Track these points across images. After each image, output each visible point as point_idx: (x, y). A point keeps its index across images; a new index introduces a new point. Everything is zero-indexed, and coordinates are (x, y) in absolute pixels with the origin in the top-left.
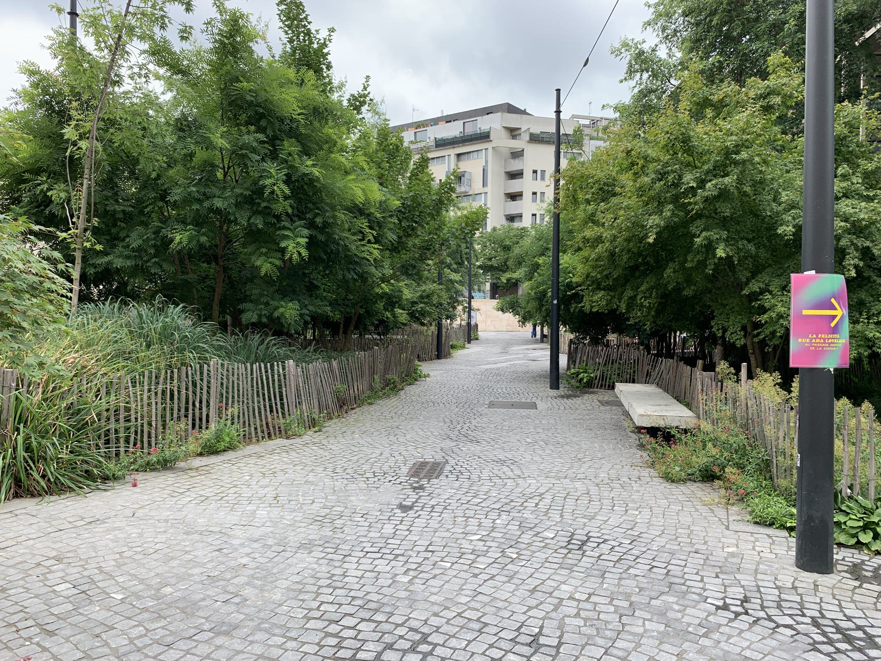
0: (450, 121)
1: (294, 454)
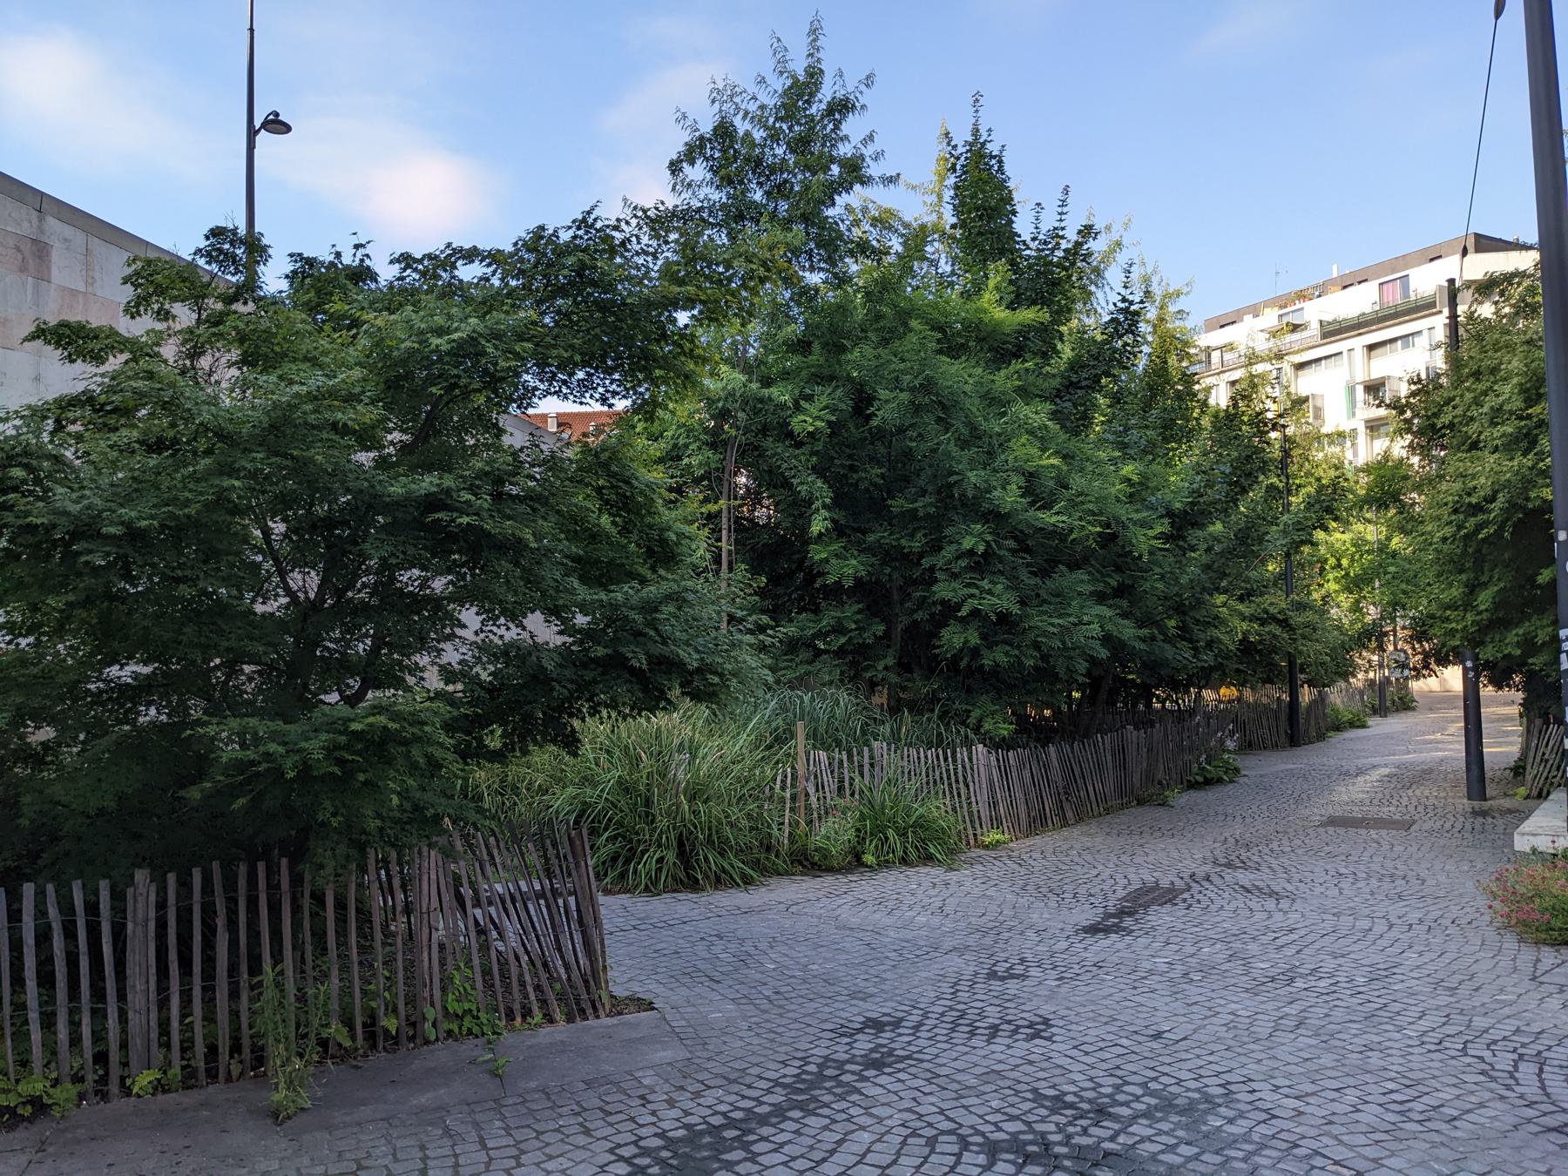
0: (1366, 280)
1: (980, 867)
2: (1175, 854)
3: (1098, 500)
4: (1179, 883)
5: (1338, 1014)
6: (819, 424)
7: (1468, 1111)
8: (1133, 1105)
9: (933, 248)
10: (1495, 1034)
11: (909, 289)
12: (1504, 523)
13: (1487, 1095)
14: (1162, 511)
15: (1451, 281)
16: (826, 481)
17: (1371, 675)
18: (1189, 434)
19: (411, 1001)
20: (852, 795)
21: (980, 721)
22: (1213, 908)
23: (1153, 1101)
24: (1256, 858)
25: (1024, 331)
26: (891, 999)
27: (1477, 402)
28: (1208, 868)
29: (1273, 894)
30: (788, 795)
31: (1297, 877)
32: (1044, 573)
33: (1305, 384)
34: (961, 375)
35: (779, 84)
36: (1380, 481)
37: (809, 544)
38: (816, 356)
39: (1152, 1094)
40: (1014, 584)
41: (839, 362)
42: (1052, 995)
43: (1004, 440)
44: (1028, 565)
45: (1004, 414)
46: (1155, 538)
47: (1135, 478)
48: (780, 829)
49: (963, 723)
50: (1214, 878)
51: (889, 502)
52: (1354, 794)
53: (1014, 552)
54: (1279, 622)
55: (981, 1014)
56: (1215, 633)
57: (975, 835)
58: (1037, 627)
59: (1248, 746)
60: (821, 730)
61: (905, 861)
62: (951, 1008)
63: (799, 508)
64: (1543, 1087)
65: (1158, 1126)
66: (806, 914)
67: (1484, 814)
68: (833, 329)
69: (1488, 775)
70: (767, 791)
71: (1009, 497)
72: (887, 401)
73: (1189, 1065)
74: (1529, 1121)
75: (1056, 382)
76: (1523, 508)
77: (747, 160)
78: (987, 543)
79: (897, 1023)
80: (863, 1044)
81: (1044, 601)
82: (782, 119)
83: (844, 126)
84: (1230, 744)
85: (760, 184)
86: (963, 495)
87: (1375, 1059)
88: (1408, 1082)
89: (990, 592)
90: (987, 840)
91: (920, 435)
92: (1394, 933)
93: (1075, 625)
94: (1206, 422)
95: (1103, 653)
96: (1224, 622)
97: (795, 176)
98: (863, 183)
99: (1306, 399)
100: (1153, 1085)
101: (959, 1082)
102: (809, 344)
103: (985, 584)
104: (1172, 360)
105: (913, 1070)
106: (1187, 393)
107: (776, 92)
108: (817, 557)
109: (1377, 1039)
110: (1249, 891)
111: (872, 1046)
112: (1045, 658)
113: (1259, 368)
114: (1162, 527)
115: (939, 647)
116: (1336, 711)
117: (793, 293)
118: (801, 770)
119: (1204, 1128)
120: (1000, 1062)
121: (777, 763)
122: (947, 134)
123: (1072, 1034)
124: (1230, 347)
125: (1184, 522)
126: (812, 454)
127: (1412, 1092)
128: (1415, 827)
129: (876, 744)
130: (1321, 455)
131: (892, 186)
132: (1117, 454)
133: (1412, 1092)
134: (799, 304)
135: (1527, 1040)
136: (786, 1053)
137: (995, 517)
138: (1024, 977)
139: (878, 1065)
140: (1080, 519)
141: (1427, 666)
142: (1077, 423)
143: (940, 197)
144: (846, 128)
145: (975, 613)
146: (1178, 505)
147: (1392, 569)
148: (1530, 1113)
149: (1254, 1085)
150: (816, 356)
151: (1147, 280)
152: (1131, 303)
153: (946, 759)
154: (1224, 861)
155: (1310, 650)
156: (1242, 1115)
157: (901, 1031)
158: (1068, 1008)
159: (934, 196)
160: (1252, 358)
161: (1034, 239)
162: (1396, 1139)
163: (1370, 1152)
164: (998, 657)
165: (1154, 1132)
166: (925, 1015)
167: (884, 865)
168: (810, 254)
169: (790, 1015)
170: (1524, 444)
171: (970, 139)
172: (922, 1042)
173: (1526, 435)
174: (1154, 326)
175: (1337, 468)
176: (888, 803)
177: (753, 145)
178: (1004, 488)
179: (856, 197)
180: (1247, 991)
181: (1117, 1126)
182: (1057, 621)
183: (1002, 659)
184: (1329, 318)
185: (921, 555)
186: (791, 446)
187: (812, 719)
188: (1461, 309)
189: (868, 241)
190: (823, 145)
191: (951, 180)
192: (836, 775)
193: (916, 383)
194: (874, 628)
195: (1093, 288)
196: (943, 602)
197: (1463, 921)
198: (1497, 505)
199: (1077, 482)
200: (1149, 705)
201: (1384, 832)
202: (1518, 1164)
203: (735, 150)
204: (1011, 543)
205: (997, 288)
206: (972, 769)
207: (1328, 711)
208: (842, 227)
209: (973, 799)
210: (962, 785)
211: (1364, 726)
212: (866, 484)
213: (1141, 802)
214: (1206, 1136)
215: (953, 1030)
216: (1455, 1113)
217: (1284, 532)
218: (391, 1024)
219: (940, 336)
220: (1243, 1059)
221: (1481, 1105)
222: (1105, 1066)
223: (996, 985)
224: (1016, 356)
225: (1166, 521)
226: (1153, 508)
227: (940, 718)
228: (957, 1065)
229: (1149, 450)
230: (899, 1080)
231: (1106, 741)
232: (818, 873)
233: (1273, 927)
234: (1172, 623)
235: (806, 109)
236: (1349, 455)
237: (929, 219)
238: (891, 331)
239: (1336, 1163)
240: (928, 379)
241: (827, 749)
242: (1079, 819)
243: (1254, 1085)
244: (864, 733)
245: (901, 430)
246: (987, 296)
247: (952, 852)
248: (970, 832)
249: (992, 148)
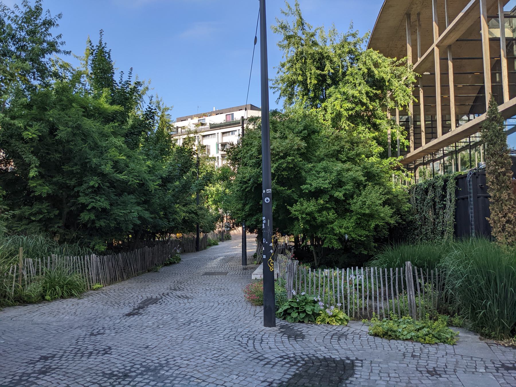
1: (91, 297)
2: (158, 287)
3: (138, 172)
4: (159, 297)
5: (202, 333)
6: (34, 136)
7: (234, 357)
8: (137, 371)
9: (84, 79)
10: (243, 333)
11: (74, 92)
12: (252, 187)
13: (240, 351)
14: (159, 177)
15: (243, 117)
16: (37, 157)
17: (220, 229)
18: (168, 153)
20: (42, 274)
21: (94, 246)
22: (169, 303)
23: (143, 369)
24: (183, 287)
25: (116, 112)
26: (52, 348)
27: (247, 153)
28: (168, 291)
29: (187, 298)
30: (14, 275)
31: (194, 291)
32: (120, 195)
33: (205, 142)
34: (89, 124)
35: (24, 10)
36: (223, 173)
37: (28, 180)
38: (34, 111)
39: (143, 367)
40: (108, 198)
41: (44, 114)
42: (113, 339)
43: (107, 149)
44: (114, 192)
45: (107, 140)
46: (157, 185)
47: (151, 166)
48: (10, 289)
49: (88, 247)
50: (170, 294)
51: (62, 167)
52: (213, 265)
53: (108, 187)
54: (194, 213)
55: (87, 349)
56: (175, 216)
57: (90, 286)
58: (116, 213)
59: (184, 252)
60: (30, 250)
61: (62, 297)
62: (75, 348)
63: (25, 167)
64: (254, 347)
65: (144, 377)
66: (19, 320)
67: (245, 269)
68: (42, 102)
69: (248, 258)
70: (5, 274)
71: (108, 168)
72: (62, 131)
73: (156, 355)
74: (250, 357)
75: (126, 131)
76: (257, 183)
77: (9, 35)
78: (99, 184)
79: (54, 356)
80: (39, 366)
81: (119, 205)
82: (24, 22)
83: (49, 30)
84: (178, 251)
85: (14, 45)
86: (91, 166)
87: (211, 345)
88: (219, 350)
89: (99, 201)
90: (95, 287)
91: (75, 144)
92: (219, 306)
93: (129, 213)
94: (174, 150)
95: (139, 222)
96: (178, 213)
97: (29, 44)
98: (56, 52)
99: (205, 146)
100: (144, 364)
101: (75, 374)
102: (32, 106)
103: (98, 198)
104: (165, 129)
105: (58, 372)
106: (169, 141)
107: (22, 12)
108: (32, 185)
109: (212, 339)
110: (180, 297)
111: (42, 366)
112: (118, 224)
113: (192, 135)
114: (159, 182)
115: (80, 220)
116: (210, 240)
117: (26, 87)
118: (20, 267)
119: (159, 375)
120: (92, 364)
121: (10, 263)
122: (90, 42)
123: (118, 351)
124: (183, 128)
125: (166, 181)
126: (31, 147)
127: (220, 353)
128: (228, 274)
129: (53, 255)
130: (208, 163)
131: (68, 55)
132: (146, 157)
133: (220, 353)
134: (28, 91)
135: (251, 334)
136: (6, 374)
137: (103, 175)
138: (103, 334)
139: (44, 373)
140: (132, 178)
141: (233, 227)
142: (134, 146)
143: (87, 62)
144: (50, 31)
145: (93, 208)
146: (164, 175)
147: (225, 198)
148: (250, 354)
149: (175, 359)
150: (34, 111)
151: (158, 103)
152: (152, 109)
153: (81, 260)
154: (173, 288)
155: (203, 223)
156: (171, 369)
157: (55, 359)
158: (118, 342)
159: (85, 62)
160: (189, 132)
161: (120, 83)
162: (215, 368)
163: (207, 374)
164: (102, 223)
165: (142, 379)
166: (65, 352)
167: (54, 299)
168: (34, 73)
169: (10, 359)
170: (257, 166)
171: (99, 45)
172: (63, 362)
173: (258, 163)
174: (160, 118)
175: (212, 168)
176: (57, 277)
177: (11, 29)
178: (106, 165)
179: (54, 56)
180: (176, 329)
181: (130, 380)
182: (123, 211)
183: (103, 224)
184: (212, 123)
185: (74, 187)
186: (23, 143)
187: (27, 246)
188: (245, 126)
189: (57, 73)
190: (41, 35)
191: (91, 57)
192: (36, 267)
193: (74, 125)
194: (54, 212)
195: (139, 102)
196: (83, 204)
197: (238, 301)
198: (251, 182)
199: (132, 165)
200: (154, 239)
201: (219, 276)
202: (246, 370)
203: (4, 30)
204: (108, 184)
205: (106, 97)
206: (90, 262)
207: (208, 240)
208: (47, 66)
209: (90, 273)
210: (86, 269)
211: (217, 245)
212: (53, 159)
213: (149, 271)
214: (159, 377)
215: (75, 356)
216: (231, 358)
217: (196, 186)
219: (84, 110)
220: (173, 351)
221: (238, 354)
222: (129, 360)
223: (93, 338)
224: (112, 121)
225: (160, 180)
226: (156, 176)
227: (79, 245)
228: (75, 368)
229: (155, 157)
230: (52, 377)
231: (138, 252)
232: (25, 304)
233: (186, 308)
234: (162, 213)
235: (34, 21)
236: (216, 164)
237: (83, 69)
238: (66, 106)
239: (197, 379)
240: (78, 124)
241: (32, 257)
242: (128, 278)
243: (175, 359)
244: (48, 251)
245: (68, 142)
246: (102, 99)
247: (81, 293)
248: (88, 285)
249: (107, 49)
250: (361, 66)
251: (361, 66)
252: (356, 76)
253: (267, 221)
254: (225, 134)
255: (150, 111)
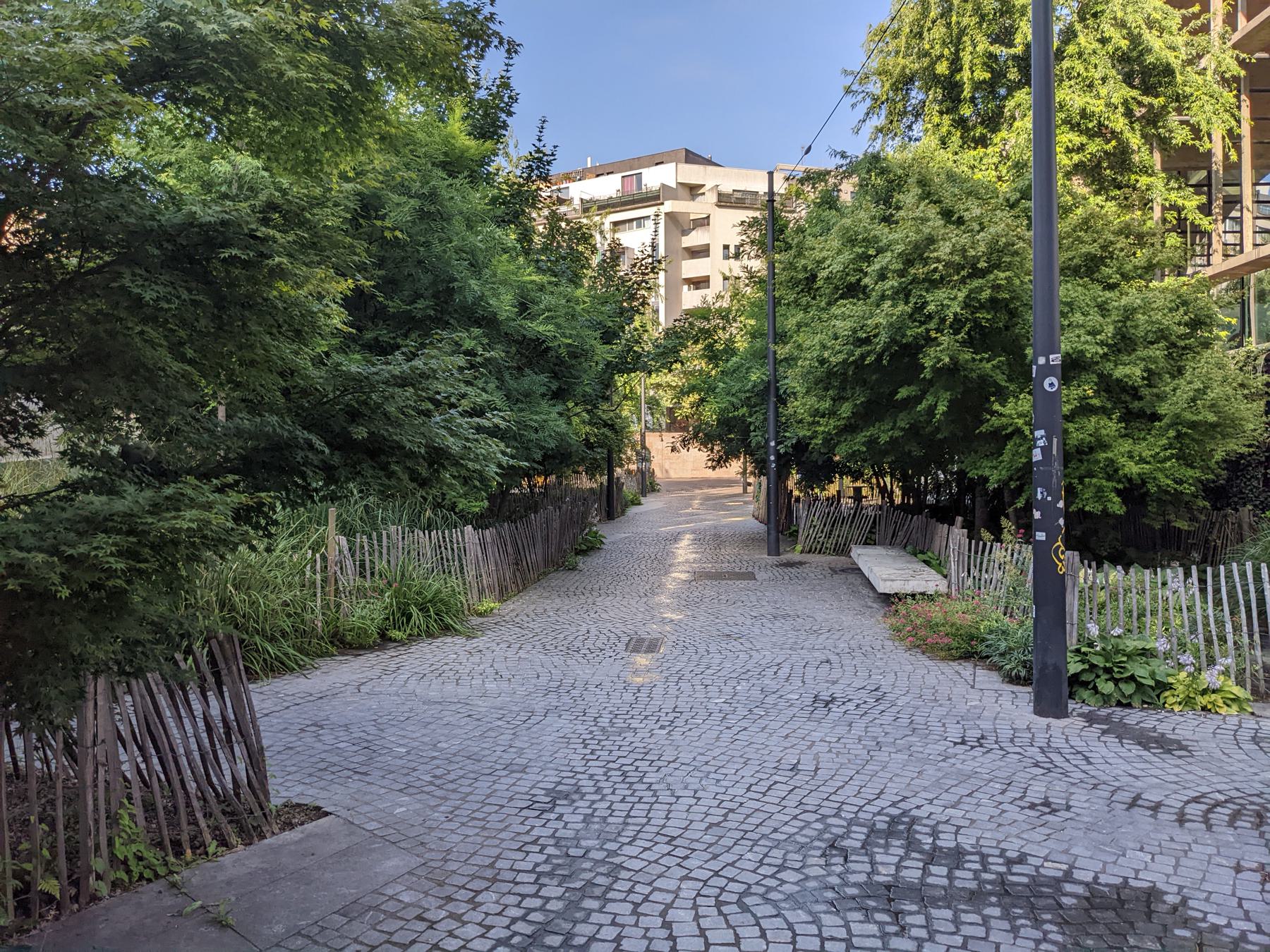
19: (73, 855)
61: (430, 635)
152: (545, 155)
211: (639, 504)
218: (51, 886)
250: (1109, 31)
251: (1109, 31)
252: (1093, 60)
253: (1049, 438)
254: (621, 227)
255: (540, 159)
